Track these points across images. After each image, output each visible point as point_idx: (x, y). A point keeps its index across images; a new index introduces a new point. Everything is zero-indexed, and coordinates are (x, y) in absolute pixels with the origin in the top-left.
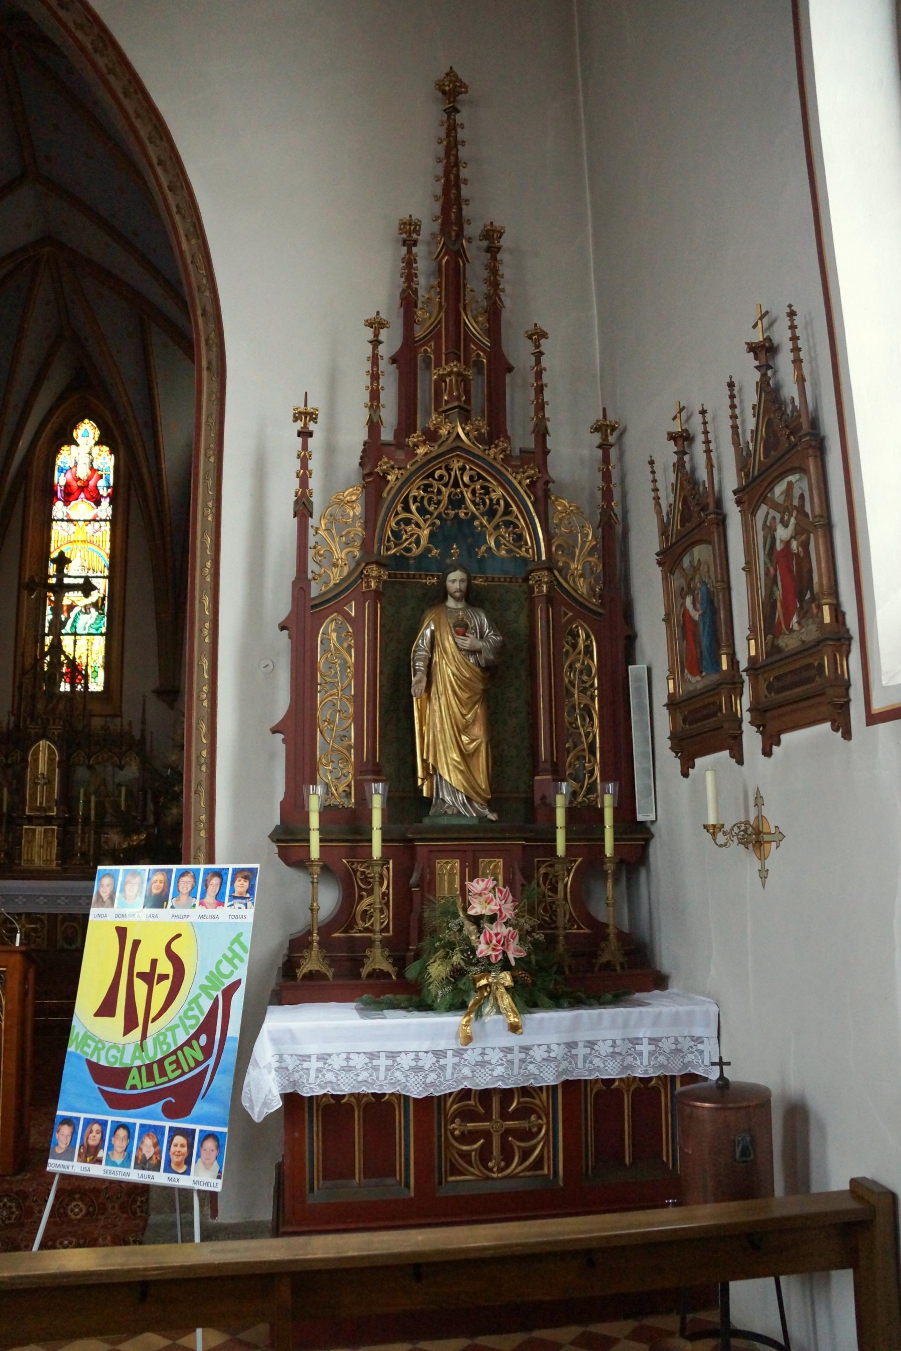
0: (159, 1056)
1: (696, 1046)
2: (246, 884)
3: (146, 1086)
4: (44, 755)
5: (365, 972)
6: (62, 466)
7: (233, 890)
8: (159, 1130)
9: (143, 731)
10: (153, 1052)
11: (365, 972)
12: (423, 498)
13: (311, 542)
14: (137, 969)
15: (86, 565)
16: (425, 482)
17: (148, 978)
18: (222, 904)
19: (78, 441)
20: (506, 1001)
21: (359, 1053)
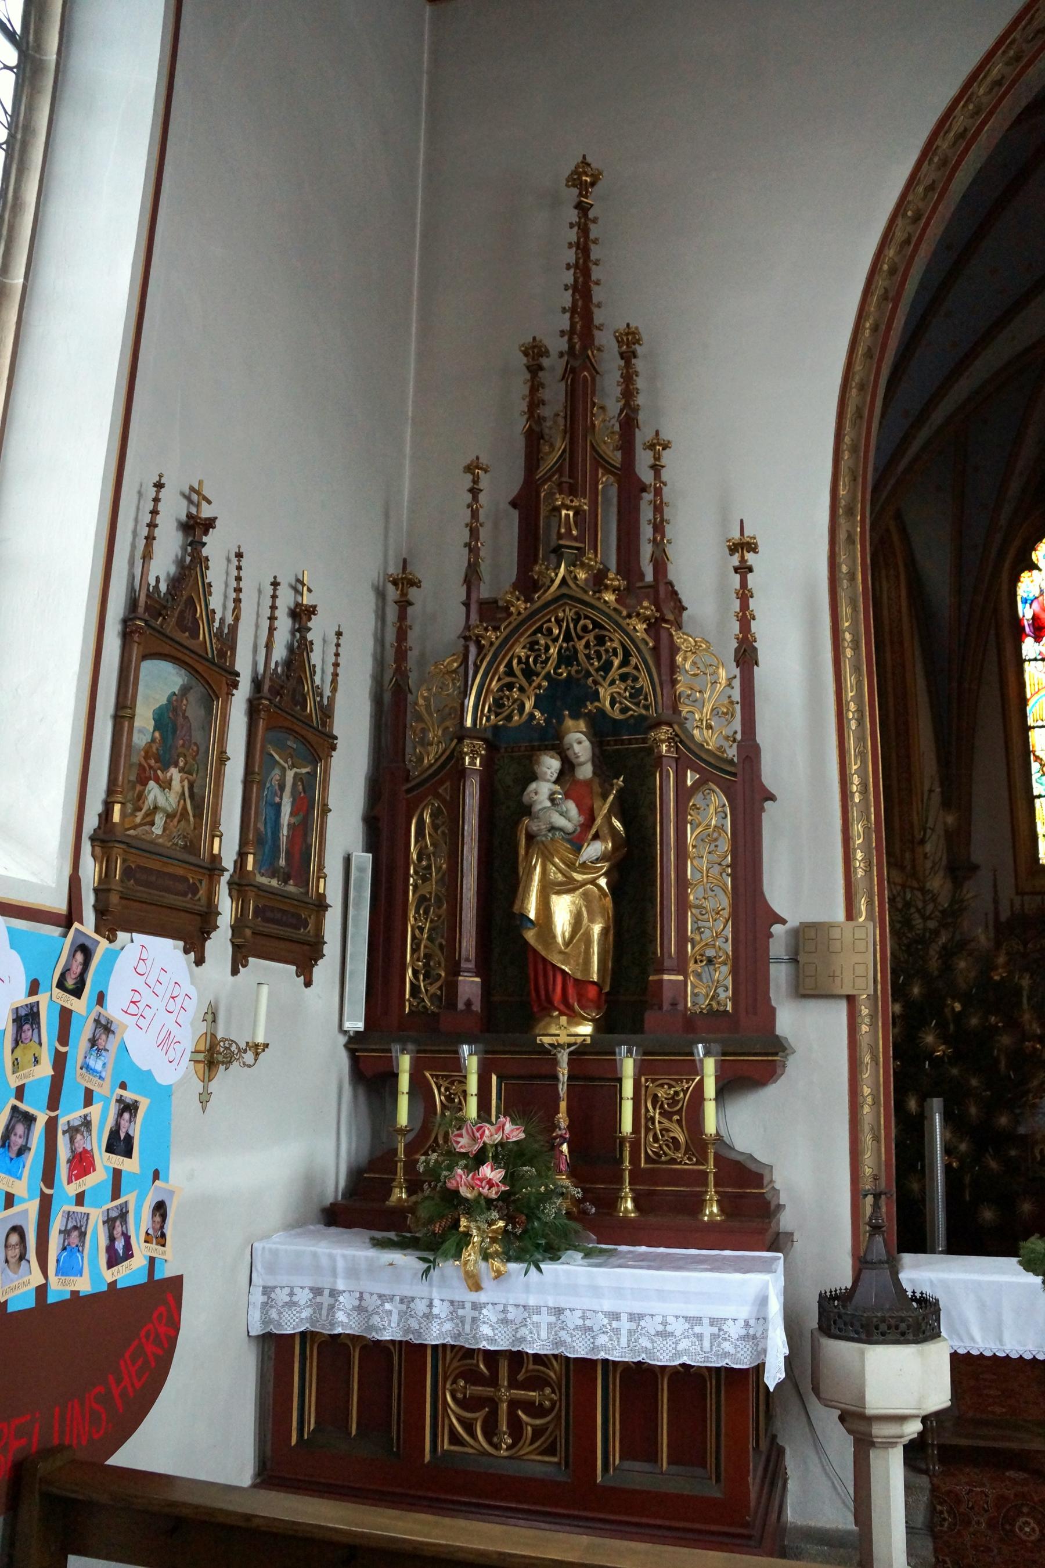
1: (693, 1329)
6: (1025, 596)
12: (528, 657)
16: (530, 639)
19: (1040, 565)
21: (303, 1288)
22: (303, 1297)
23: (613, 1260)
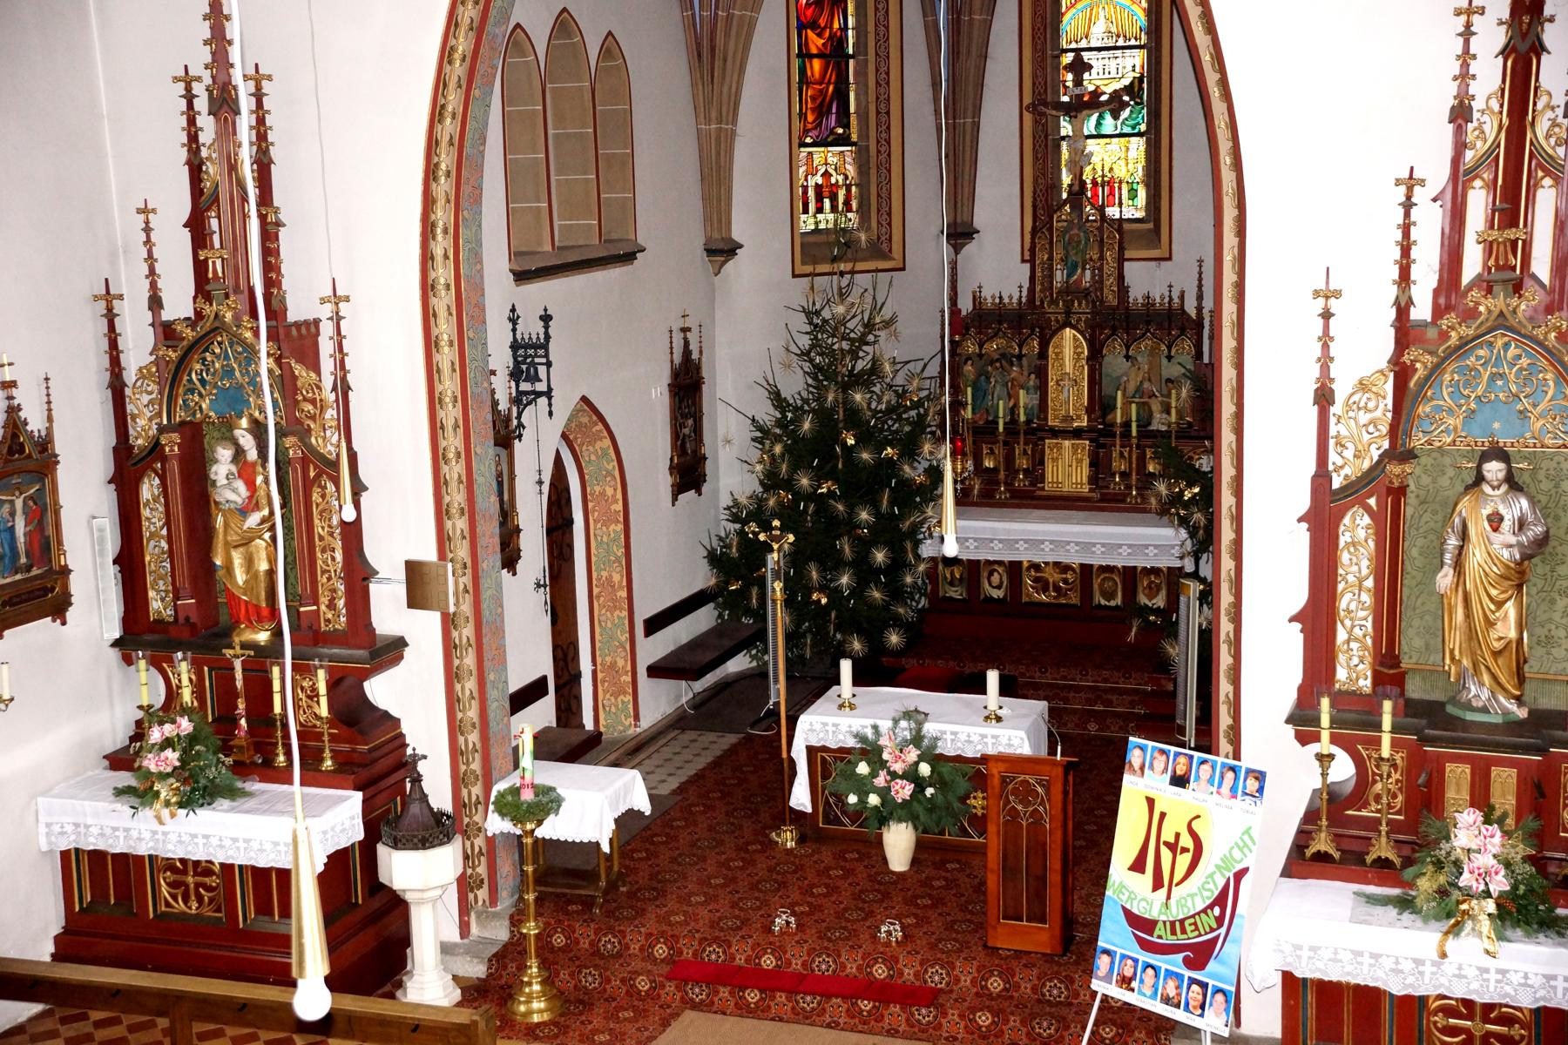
0: (1181, 917)
2: (1257, 785)
3: (1169, 940)
4: (1069, 345)
5: (1369, 859)
7: (1245, 787)
8: (1179, 977)
9: (1199, 309)
10: (1176, 913)
11: (1369, 859)
13: (1333, 431)
14: (1163, 839)
15: (1114, 30)
17: (1172, 847)
18: (1234, 797)
20: (1485, 925)
22: (69, 828)
23: (250, 803)
